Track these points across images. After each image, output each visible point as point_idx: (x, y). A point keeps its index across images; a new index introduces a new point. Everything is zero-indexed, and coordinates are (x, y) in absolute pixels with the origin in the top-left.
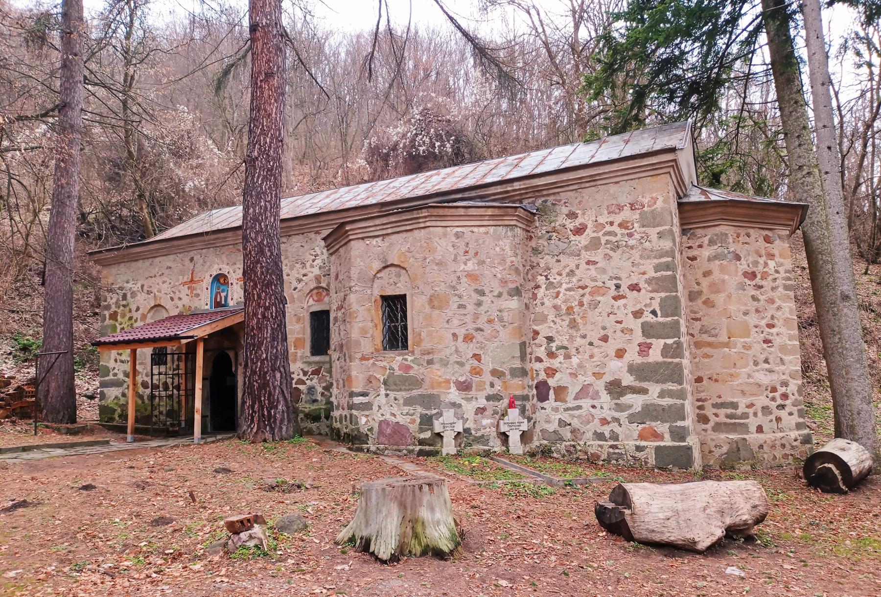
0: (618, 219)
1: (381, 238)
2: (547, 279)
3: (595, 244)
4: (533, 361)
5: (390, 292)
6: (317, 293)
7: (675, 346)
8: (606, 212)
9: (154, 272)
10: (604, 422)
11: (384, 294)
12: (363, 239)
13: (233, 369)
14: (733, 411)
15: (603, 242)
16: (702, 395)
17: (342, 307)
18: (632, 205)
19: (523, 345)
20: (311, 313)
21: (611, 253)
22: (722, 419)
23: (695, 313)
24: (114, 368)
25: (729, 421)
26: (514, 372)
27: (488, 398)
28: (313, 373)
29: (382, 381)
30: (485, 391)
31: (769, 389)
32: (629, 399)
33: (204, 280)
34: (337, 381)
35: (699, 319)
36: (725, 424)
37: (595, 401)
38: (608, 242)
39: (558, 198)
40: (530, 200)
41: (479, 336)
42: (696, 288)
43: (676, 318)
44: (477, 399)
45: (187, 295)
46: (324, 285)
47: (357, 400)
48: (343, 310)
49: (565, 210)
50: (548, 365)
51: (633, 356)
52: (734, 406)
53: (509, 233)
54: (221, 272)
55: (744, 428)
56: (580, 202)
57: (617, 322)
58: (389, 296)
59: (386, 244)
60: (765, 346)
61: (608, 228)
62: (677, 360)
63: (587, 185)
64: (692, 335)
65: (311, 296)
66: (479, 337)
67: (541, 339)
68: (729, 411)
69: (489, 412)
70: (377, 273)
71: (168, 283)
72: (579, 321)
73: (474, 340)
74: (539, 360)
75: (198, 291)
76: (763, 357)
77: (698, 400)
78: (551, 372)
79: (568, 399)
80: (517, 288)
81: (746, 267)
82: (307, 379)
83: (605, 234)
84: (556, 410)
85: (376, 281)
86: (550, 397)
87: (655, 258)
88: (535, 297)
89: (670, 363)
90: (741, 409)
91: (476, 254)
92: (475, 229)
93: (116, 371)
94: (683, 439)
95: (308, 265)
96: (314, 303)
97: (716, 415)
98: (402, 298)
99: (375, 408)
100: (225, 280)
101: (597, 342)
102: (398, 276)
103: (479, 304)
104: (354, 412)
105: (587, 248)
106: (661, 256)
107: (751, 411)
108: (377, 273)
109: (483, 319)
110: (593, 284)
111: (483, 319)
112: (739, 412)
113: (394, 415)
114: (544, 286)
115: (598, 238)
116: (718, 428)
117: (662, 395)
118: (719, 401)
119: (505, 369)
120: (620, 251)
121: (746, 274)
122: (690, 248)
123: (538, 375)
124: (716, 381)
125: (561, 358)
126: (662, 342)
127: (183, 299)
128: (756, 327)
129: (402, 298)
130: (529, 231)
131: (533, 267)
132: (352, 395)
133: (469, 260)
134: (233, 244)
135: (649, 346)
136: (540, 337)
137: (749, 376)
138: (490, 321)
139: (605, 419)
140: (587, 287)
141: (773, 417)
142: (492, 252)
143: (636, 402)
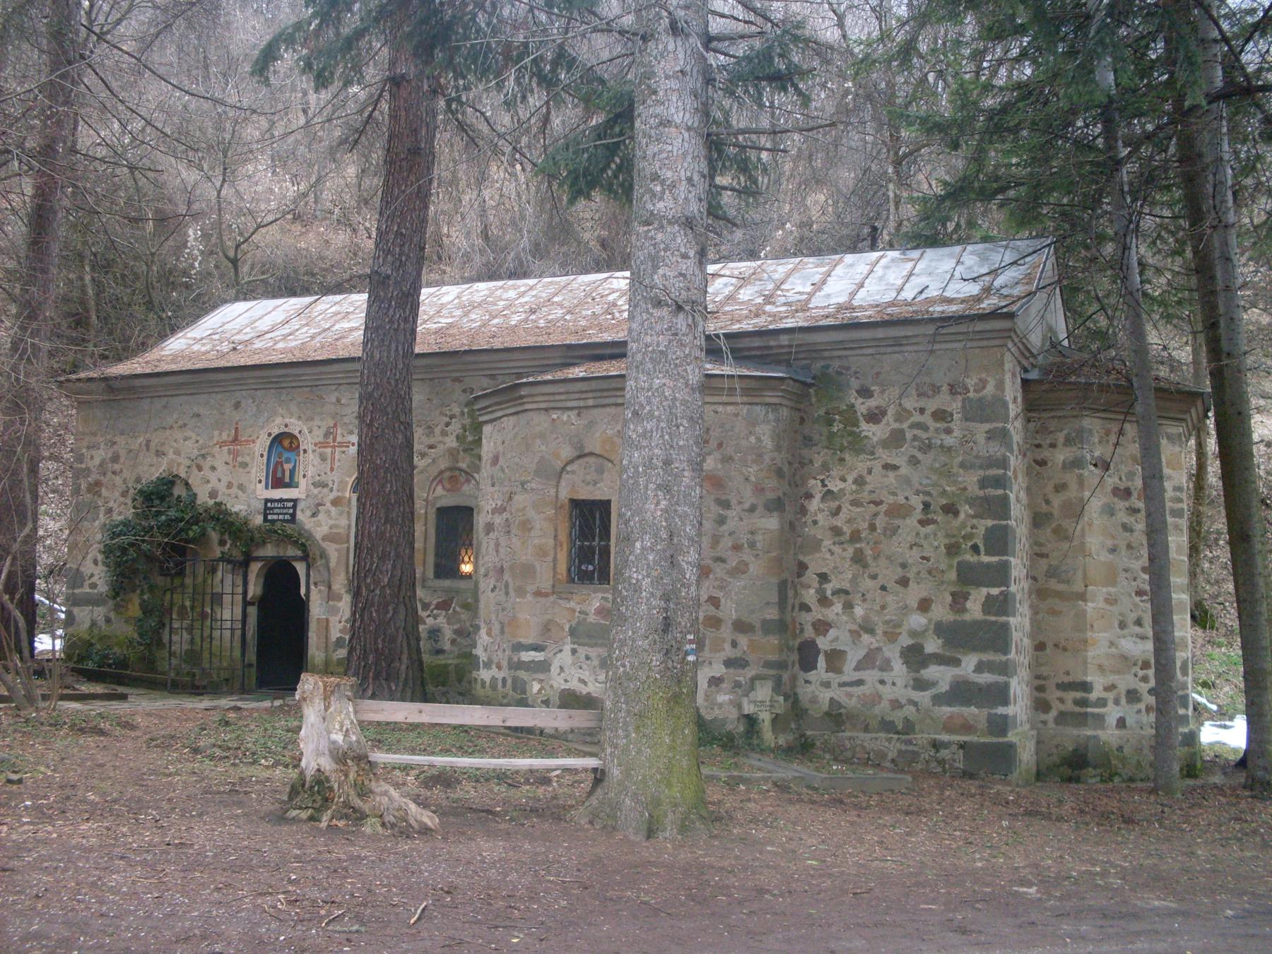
0: (932, 405)
1: (576, 412)
2: (824, 485)
3: (896, 439)
4: (797, 609)
5: (585, 494)
6: (451, 477)
8: (914, 392)
9: (170, 421)
10: (896, 705)
12: (546, 410)
13: (303, 591)
14: (1085, 695)
15: (909, 435)
16: (1044, 670)
17: (505, 510)
18: (951, 386)
19: (783, 587)
20: (438, 509)
21: (919, 456)
22: (1069, 706)
23: (1041, 545)
24: (92, 575)
25: (1078, 709)
26: (768, 627)
27: (729, 663)
28: (438, 607)
29: (567, 628)
30: (723, 653)
33: (258, 442)
34: (488, 623)
35: (1047, 556)
36: (1072, 714)
38: (915, 438)
39: (846, 364)
40: (804, 362)
41: (719, 570)
44: (710, 663)
46: (463, 465)
47: (527, 656)
48: (505, 515)
49: (855, 384)
50: (820, 617)
51: (941, 612)
52: (1085, 687)
53: (771, 416)
54: (286, 430)
56: (878, 374)
57: (923, 558)
60: (1137, 599)
61: (917, 418)
62: (1004, 619)
63: (889, 350)
65: (440, 481)
66: (718, 570)
67: (810, 577)
70: (567, 464)
71: (193, 441)
72: (868, 552)
73: (711, 576)
74: (805, 608)
75: (247, 459)
76: (1133, 616)
77: (1037, 677)
78: (822, 627)
80: (779, 499)
81: (1117, 480)
83: (912, 426)
84: (827, 685)
85: (565, 476)
87: (981, 467)
88: (803, 511)
91: (720, 445)
92: (720, 409)
93: (94, 580)
94: (1003, 732)
95: (437, 431)
96: (444, 493)
97: (1062, 700)
98: (605, 506)
99: (554, 669)
101: (891, 585)
102: (600, 471)
103: (721, 521)
105: (885, 444)
106: (989, 466)
107: (1110, 696)
108: (567, 464)
109: (727, 542)
110: (891, 499)
111: (727, 542)
112: (1094, 696)
113: (585, 683)
114: (818, 497)
115: (902, 431)
116: (1062, 718)
118: (1067, 679)
119: (755, 619)
120: (931, 455)
121: (1116, 492)
122: (1038, 446)
123: (802, 631)
124: (1065, 649)
125: (838, 607)
128: (1126, 570)
129: (605, 506)
130: (799, 410)
131: (802, 465)
132: (519, 647)
133: (709, 454)
135: (966, 597)
137: (1112, 644)
138: (737, 548)
139: (897, 701)
140: (881, 502)
142: (744, 443)
143: (942, 676)
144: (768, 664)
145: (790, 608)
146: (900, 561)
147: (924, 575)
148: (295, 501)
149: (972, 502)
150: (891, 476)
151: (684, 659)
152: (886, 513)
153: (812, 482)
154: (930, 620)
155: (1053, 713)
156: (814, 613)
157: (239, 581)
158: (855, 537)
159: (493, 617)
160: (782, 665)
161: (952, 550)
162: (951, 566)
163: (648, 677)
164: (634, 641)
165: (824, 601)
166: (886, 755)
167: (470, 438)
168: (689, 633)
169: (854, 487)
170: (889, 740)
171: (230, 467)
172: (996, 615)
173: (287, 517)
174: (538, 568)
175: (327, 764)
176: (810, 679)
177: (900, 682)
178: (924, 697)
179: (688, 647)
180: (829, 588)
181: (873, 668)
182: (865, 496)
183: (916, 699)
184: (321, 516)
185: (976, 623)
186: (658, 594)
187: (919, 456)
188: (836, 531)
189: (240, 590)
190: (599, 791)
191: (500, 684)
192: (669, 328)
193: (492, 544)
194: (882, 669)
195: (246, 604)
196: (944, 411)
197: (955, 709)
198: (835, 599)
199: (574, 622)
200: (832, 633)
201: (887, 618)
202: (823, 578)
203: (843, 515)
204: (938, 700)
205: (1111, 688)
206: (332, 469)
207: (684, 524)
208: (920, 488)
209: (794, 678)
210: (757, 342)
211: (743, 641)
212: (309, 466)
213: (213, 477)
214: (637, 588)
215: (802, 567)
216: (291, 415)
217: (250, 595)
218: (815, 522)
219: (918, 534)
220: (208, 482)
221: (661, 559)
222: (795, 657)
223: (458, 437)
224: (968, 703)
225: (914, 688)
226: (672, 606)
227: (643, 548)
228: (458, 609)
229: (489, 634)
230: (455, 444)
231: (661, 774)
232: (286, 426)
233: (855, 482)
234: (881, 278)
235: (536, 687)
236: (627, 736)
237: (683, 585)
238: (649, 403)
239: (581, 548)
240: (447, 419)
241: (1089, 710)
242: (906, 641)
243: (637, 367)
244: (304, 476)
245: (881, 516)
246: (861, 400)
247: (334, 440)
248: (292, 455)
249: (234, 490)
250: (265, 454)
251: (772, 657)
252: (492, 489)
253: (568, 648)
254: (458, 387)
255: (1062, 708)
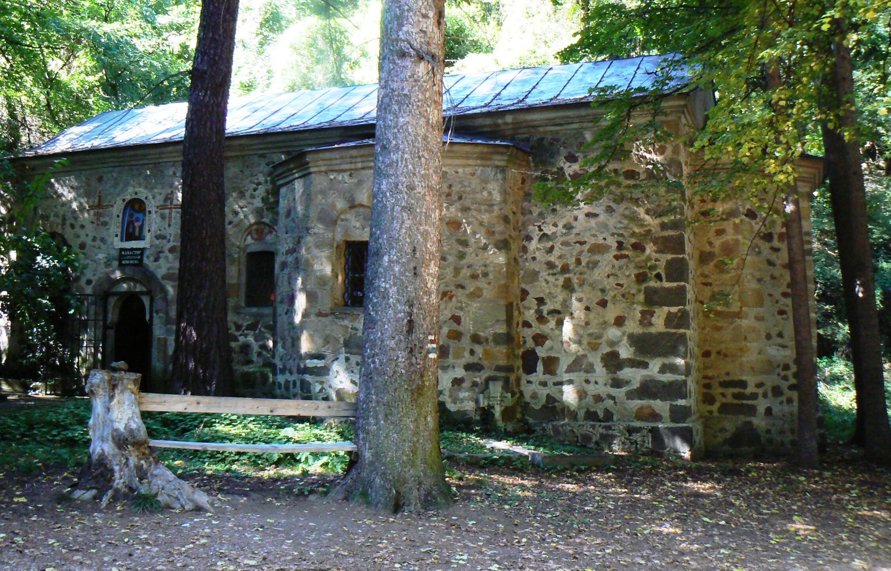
2: (541, 230)
4: (520, 326)
7: (679, 314)
10: (598, 399)
11: (349, 239)
13: (147, 317)
14: (742, 390)
16: (710, 373)
19: (509, 308)
21: (614, 206)
22: (729, 400)
25: (736, 401)
27: (468, 367)
28: (249, 328)
31: (782, 366)
32: (626, 373)
33: (115, 206)
36: (732, 405)
37: (589, 375)
42: (707, 248)
43: (682, 283)
44: (454, 367)
45: (92, 223)
51: (633, 326)
52: (743, 384)
53: (499, 176)
54: (136, 197)
55: (752, 410)
58: (354, 242)
59: (354, 180)
60: (779, 317)
62: (682, 331)
64: (702, 303)
67: (531, 301)
68: (737, 390)
69: (466, 385)
72: (575, 281)
74: (527, 324)
75: (107, 219)
79: (558, 372)
82: (241, 335)
84: (544, 384)
86: (538, 369)
88: (525, 249)
89: (675, 333)
90: (750, 389)
91: (460, 198)
95: (248, 194)
96: (253, 241)
97: (723, 395)
100: (140, 206)
103: (462, 256)
104: (308, 378)
107: (760, 391)
109: (466, 272)
110: (593, 241)
111: (466, 272)
117: (664, 369)
118: (727, 379)
123: (525, 342)
125: (552, 324)
126: (666, 309)
127: (87, 227)
134: (155, 164)
135: (652, 314)
136: (529, 297)
138: (474, 277)
140: (585, 243)
141: (784, 399)
144: (498, 368)
145: (515, 325)
146: (600, 287)
147: (619, 298)
148: (142, 250)
149: (655, 241)
150: (593, 222)
151: (426, 356)
152: (589, 251)
153: (531, 228)
154: (624, 334)
155: (717, 405)
156: (534, 329)
157: (100, 311)
158: (565, 269)
159: (286, 333)
160: (509, 369)
161: (641, 278)
162: (640, 291)
163: (394, 372)
164: (382, 341)
165: (541, 319)
166: (591, 438)
167: (272, 200)
168: (430, 334)
169: (564, 231)
170: (593, 427)
171: (95, 225)
172: (675, 328)
173: (136, 262)
174: (319, 295)
175: (109, 448)
176: (531, 379)
177: (601, 381)
178: (620, 393)
179: (430, 346)
180: (545, 309)
181: (580, 371)
182: (572, 238)
183: (614, 395)
184: (162, 261)
185: (661, 335)
186: (404, 299)
187: (614, 206)
188: (550, 265)
189: (101, 318)
190: (354, 472)
191: (291, 386)
192: (412, 76)
193: (286, 278)
194: (587, 371)
195: (106, 327)
196: (633, 171)
197: (644, 402)
198: (549, 318)
199: (348, 336)
200: (548, 343)
201: (591, 331)
202: (541, 301)
203: (557, 252)
204: (630, 395)
205: (760, 385)
206: (169, 225)
207: (426, 240)
208: (615, 231)
209: (518, 380)
210: (488, 121)
211: (479, 350)
212: (153, 223)
213: (82, 233)
214: (385, 295)
215: (525, 293)
216: (140, 186)
217: (109, 321)
218: (534, 259)
219: (613, 266)
220: (79, 237)
221: (406, 270)
222: (519, 363)
223: (263, 199)
224: (653, 396)
225: (612, 386)
226: (415, 310)
227: (390, 261)
228: (263, 329)
229: (283, 347)
230: (260, 205)
231: (407, 455)
232: (136, 193)
233: (565, 226)
234: (581, 80)
235: (318, 387)
236: (376, 424)
237: (425, 293)
238: (395, 138)
239: (354, 278)
240: (255, 186)
241: (745, 402)
242: (606, 350)
243: (385, 109)
244: (149, 231)
245: (585, 253)
246: (568, 164)
247: (171, 204)
248: (140, 215)
249: (98, 243)
250: (121, 215)
251: (502, 362)
252: (286, 236)
253: (342, 357)
254: (263, 162)
255: (724, 400)
